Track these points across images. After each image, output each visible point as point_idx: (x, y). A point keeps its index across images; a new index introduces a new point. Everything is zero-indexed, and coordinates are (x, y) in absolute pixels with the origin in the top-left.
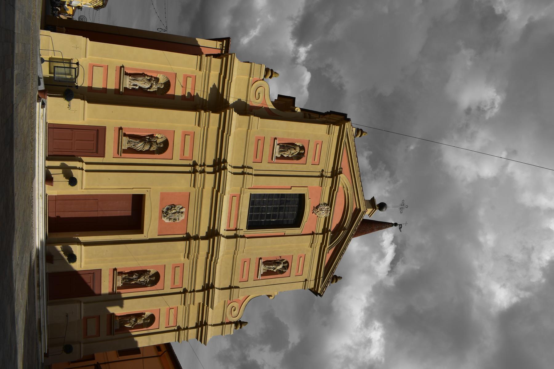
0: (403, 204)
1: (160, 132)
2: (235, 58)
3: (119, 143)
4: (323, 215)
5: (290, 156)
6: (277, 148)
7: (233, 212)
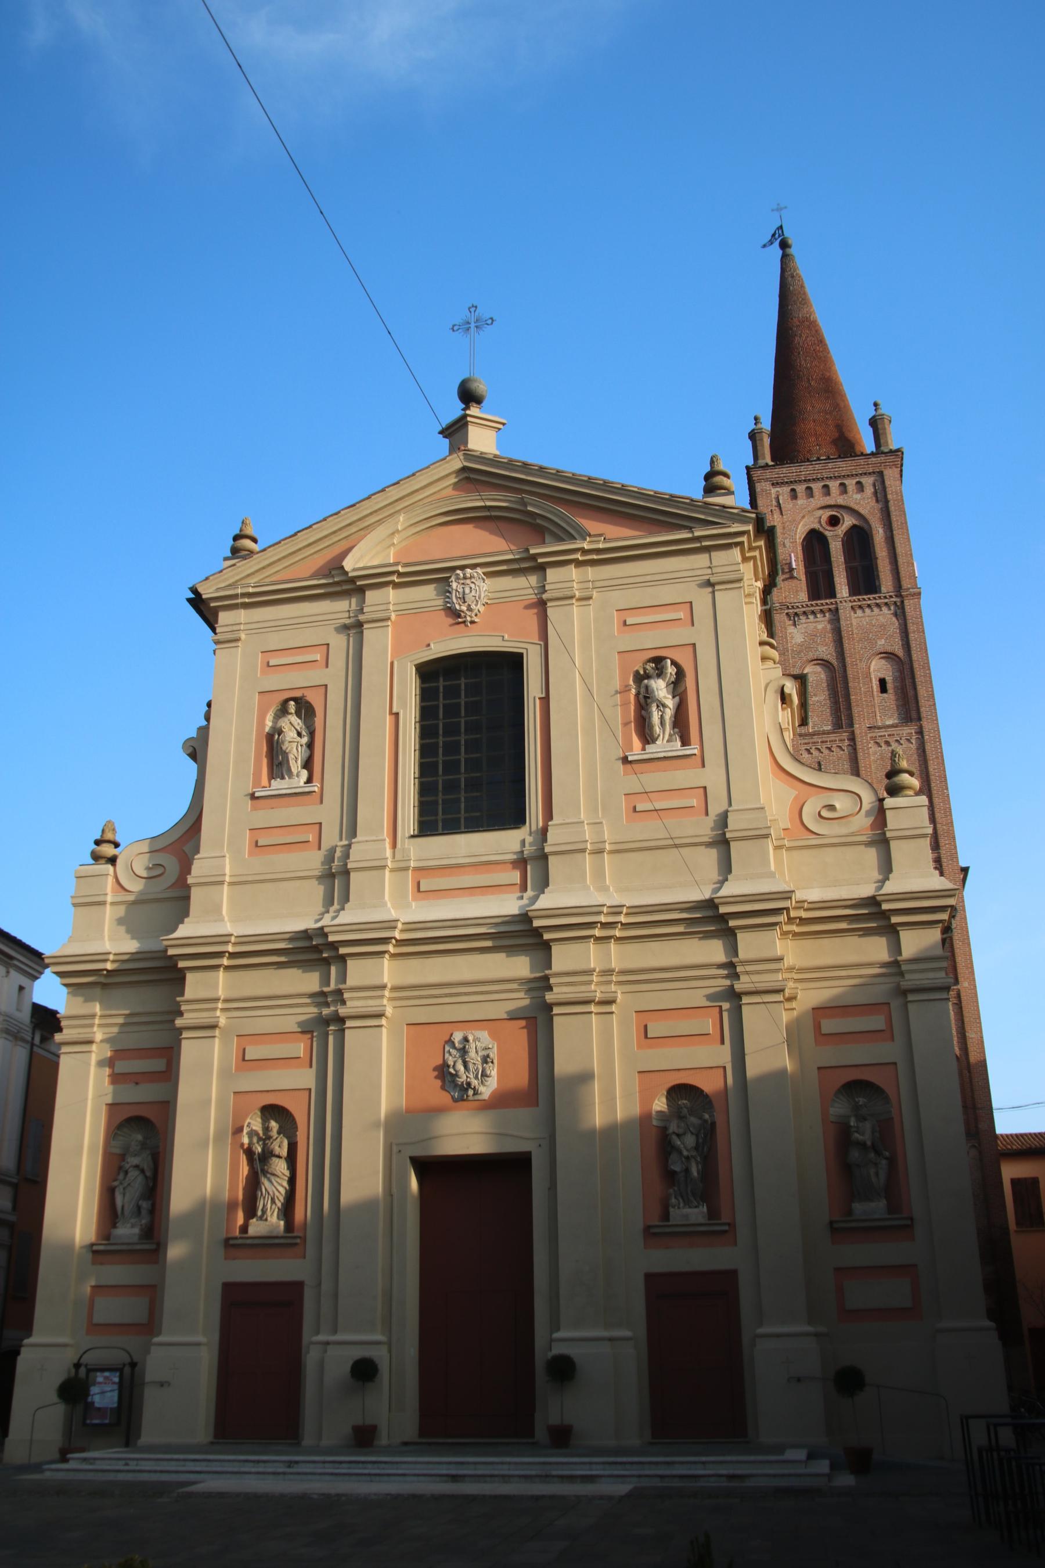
0: (465, 327)
3: (690, 1235)
5: (305, 740)
6: (279, 786)
7: (473, 876)
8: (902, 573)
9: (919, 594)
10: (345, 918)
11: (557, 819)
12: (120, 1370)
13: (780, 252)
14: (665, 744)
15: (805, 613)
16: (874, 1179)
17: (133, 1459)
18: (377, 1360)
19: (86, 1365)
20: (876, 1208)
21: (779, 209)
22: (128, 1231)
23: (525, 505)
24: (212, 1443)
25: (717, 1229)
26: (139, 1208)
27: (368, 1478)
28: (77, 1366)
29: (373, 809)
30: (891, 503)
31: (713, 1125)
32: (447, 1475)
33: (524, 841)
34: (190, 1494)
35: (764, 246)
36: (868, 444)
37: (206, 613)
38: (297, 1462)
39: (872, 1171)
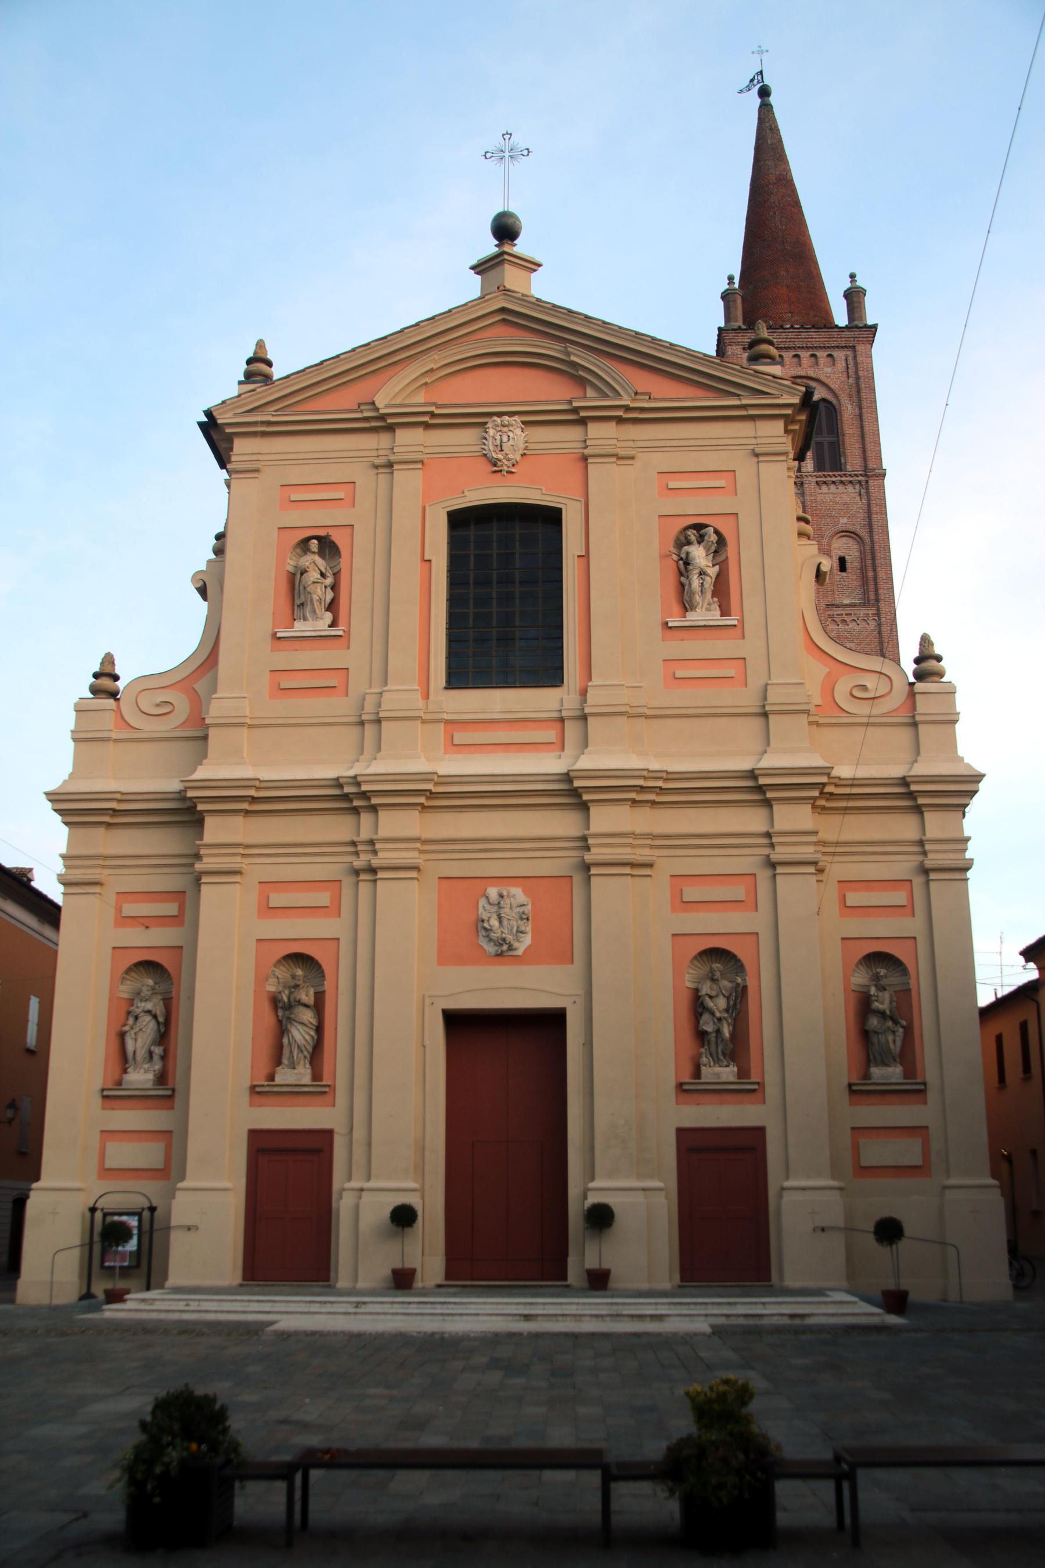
1: (261, 979)
2: (193, 777)
3: (720, 1092)
4: (517, 437)
6: (301, 628)
7: (507, 735)
8: (869, 453)
9: (884, 475)
10: (379, 767)
11: (595, 681)
12: (139, 1214)
13: (758, 101)
14: (705, 613)
16: (892, 1046)
17: (195, 1300)
19: (102, 1210)
21: (760, 52)
22: (141, 1077)
23: (568, 354)
24: (241, 1285)
25: (748, 1088)
26: (151, 1054)
27: (441, 1318)
29: (404, 659)
31: (745, 988)
32: (520, 1315)
33: (562, 699)
36: (841, 318)
37: (215, 437)
38: (365, 1303)
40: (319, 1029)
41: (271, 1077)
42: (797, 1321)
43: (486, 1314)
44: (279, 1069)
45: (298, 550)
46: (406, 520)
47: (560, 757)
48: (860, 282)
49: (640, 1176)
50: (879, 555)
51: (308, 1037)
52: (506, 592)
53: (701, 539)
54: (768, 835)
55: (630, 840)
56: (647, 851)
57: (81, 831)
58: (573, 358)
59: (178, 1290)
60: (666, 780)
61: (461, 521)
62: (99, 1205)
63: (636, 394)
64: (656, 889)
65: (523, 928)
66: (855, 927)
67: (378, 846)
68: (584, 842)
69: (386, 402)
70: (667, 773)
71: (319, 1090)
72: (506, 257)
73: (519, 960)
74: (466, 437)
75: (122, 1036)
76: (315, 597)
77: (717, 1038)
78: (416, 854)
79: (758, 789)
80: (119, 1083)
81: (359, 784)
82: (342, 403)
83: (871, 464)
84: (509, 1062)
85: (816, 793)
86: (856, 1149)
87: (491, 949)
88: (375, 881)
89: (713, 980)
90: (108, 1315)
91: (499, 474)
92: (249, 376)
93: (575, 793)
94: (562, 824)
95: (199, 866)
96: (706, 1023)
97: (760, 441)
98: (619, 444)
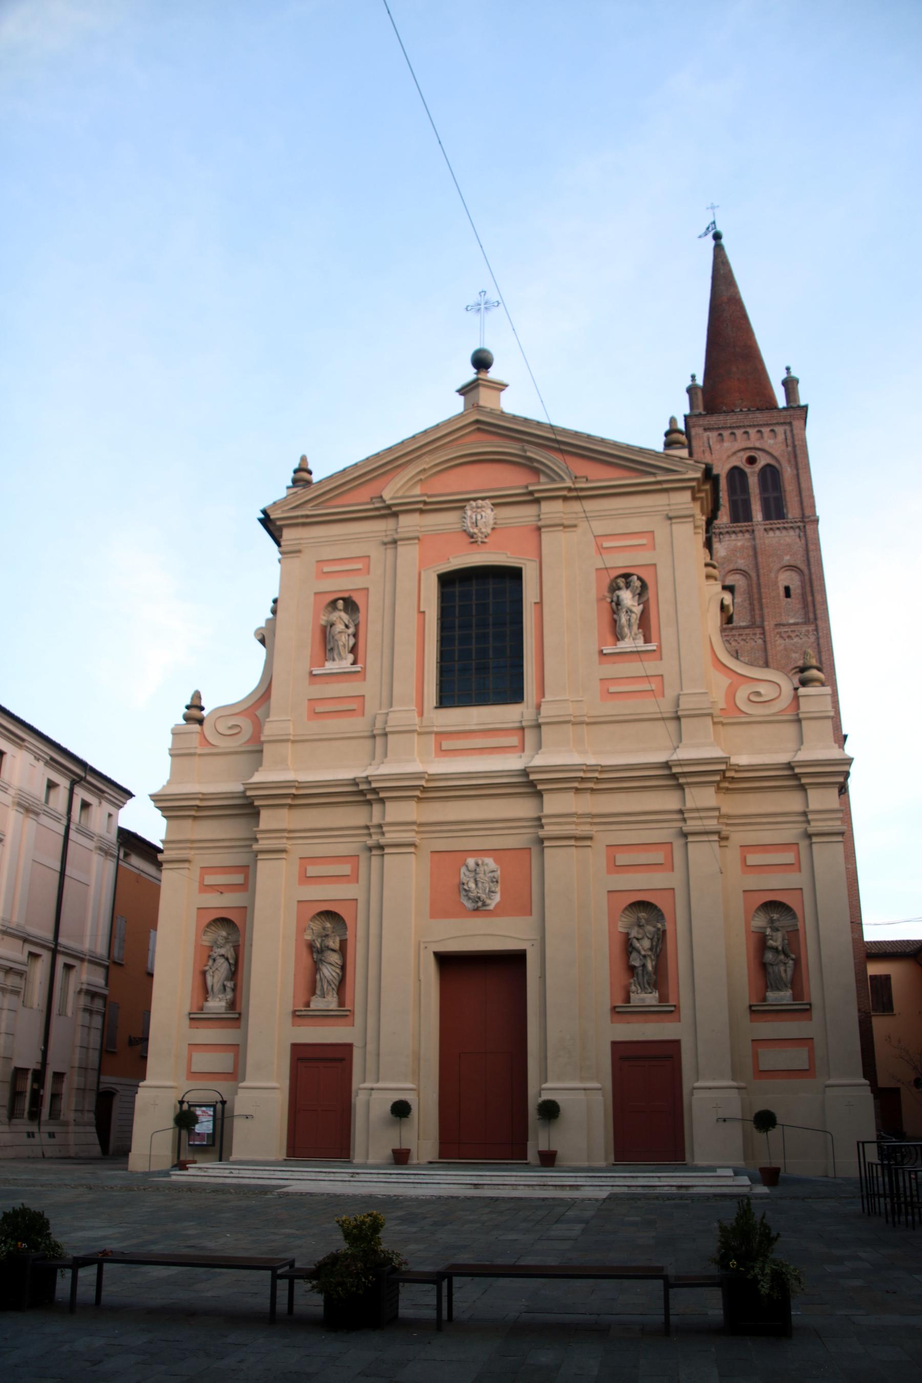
1: (301, 931)
3: (645, 1013)
4: (488, 515)
6: (331, 667)
7: (483, 743)
8: (805, 504)
10: (385, 769)
11: (548, 698)
15: (728, 532)
16: (783, 975)
18: (410, 1103)
20: (784, 996)
22: (216, 1004)
23: (525, 451)
26: (224, 986)
28: (181, 1102)
29: (405, 687)
30: (798, 448)
31: (664, 932)
33: (522, 713)
34: (287, 1194)
35: (700, 237)
36: (782, 402)
37: (272, 528)
39: (782, 968)
40: (343, 968)
41: (308, 1004)
42: (683, 1191)
43: (453, 1183)
44: (313, 998)
45: (330, 609)
46: (406, 583)
47: (521, 757)
48: (794, 373)
49: (582, 1079)
50: (816, 583)
51: (334, 974)
52: (482, 636)
53: (628, 585)
54: (681, 812)
55: (575, 819)
56: (587, 827)
57: (176, 823)
58: (529, 454)
59: (234, 1163)
60: (601, 772)
61: (447, 581)
62: (185, 1099)
63: (576, 478)
64: (594, 858)
65: (493, 889)
66: (755, 882)
67: (385, 829)
68: (539, 822)
69: (390, 495)
70: (602, 766)
71: (343, 1014)
72: (480, 382)
73: (490, 913)
74: (449, 519)
75: (204, 973)
76: (341, 643)
77: (643, 971)
78: (413, 834)
79: (672, 777)
80: (201, 1008)
81: (369, 783)
82: (360, 498)
83: (808, 512)
84: (484, 988)
85: (717, 778)
86: (755, 1056)
87: (469, 905)
88: (383, 855)
89: (640, 926)
90: (174, 1178)
91: (475, 545)
92: (295, 482)
93: (532, 784)
94: (522, 808)
95: (256, 847)
96: (635, 960)
97: (672, 507)
98: (565, 516)
